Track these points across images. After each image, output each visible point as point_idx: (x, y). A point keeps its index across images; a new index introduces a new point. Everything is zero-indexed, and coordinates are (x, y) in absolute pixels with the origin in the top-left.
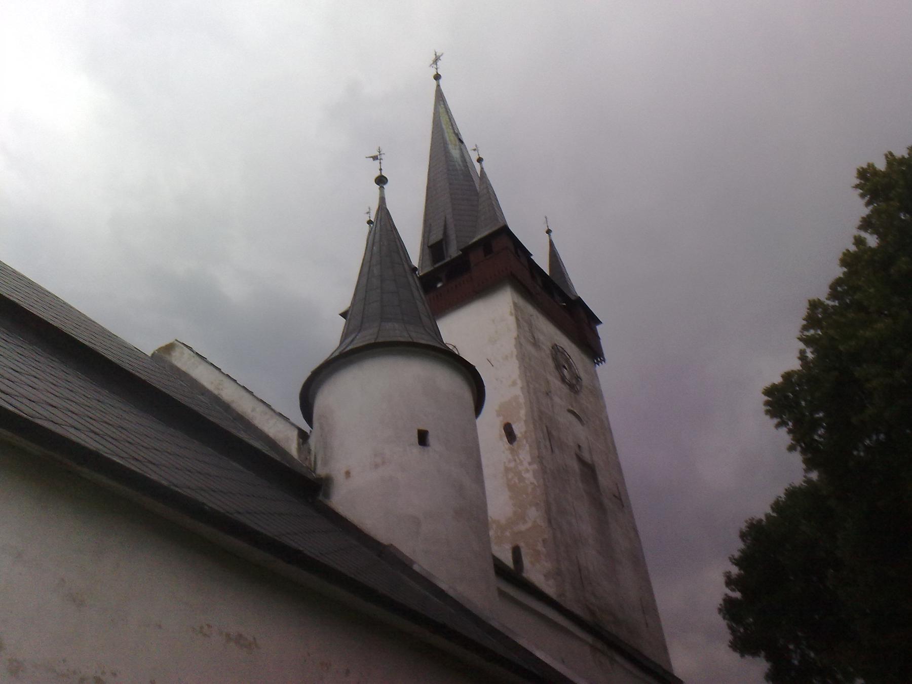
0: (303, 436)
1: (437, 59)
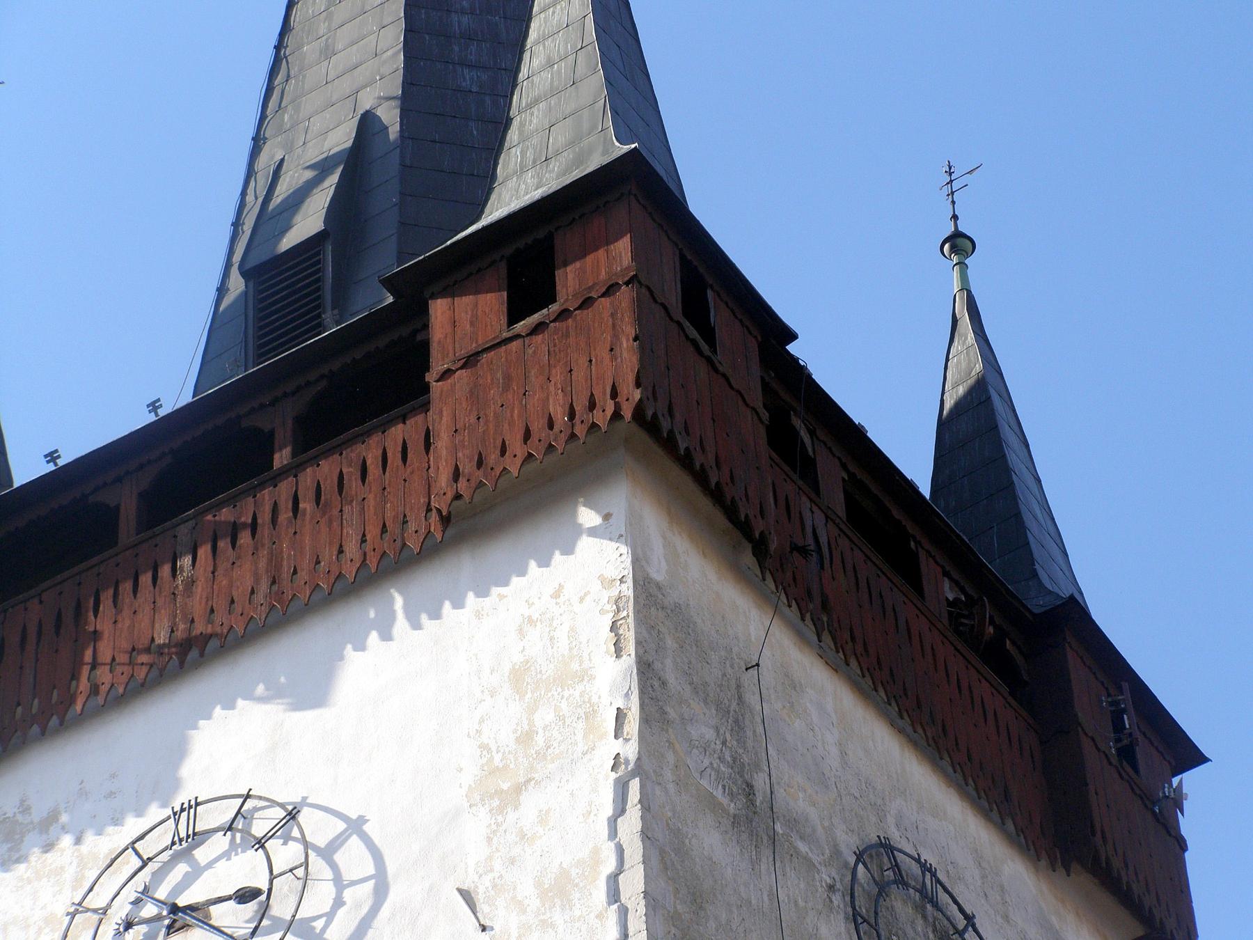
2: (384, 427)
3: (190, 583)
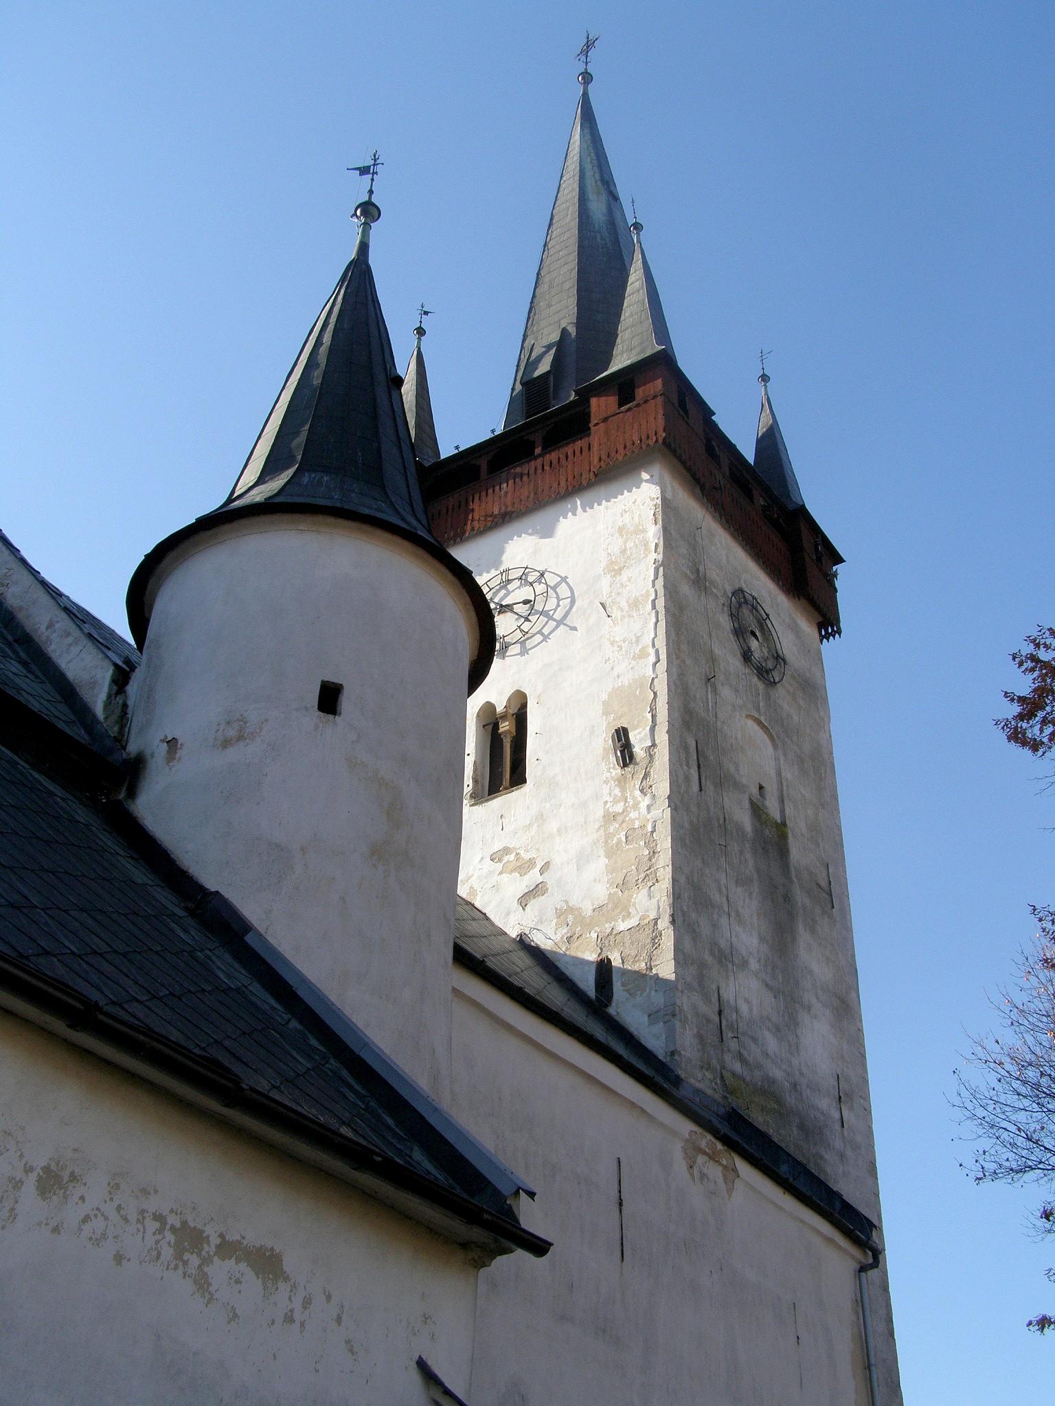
0: (122, 677)
1: (589, 45)
2: (574, 442)
3: (506, 493)
